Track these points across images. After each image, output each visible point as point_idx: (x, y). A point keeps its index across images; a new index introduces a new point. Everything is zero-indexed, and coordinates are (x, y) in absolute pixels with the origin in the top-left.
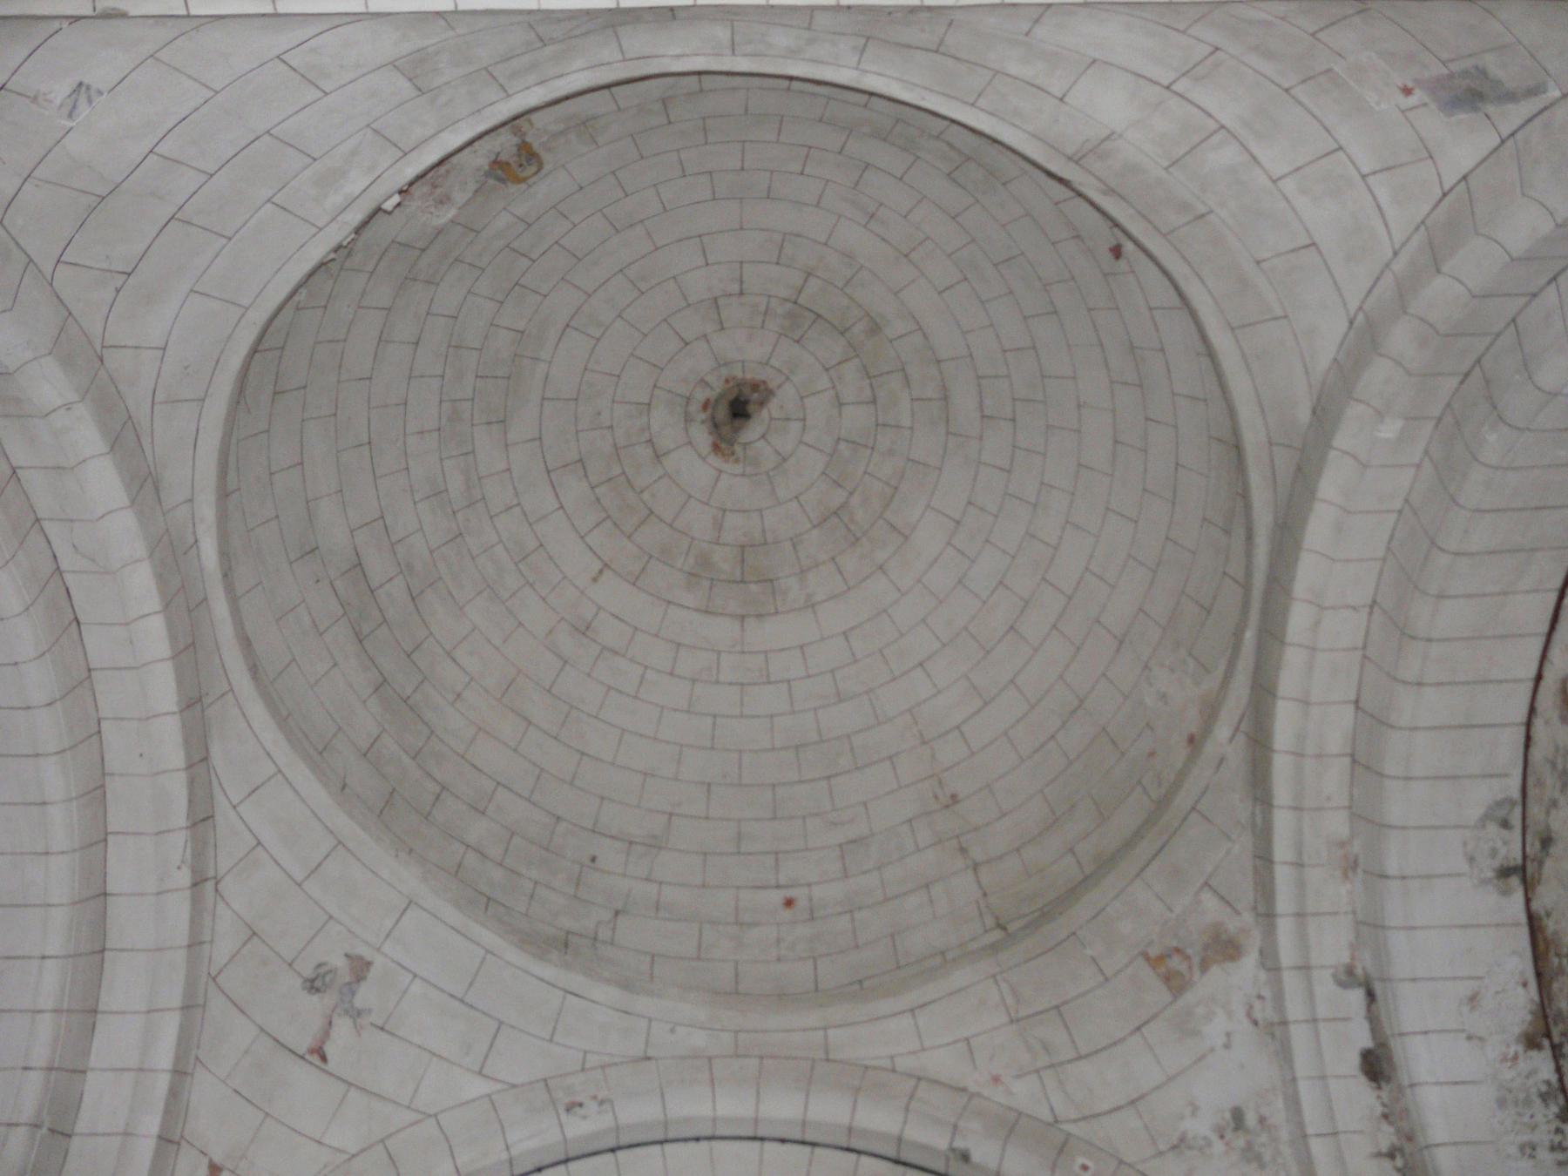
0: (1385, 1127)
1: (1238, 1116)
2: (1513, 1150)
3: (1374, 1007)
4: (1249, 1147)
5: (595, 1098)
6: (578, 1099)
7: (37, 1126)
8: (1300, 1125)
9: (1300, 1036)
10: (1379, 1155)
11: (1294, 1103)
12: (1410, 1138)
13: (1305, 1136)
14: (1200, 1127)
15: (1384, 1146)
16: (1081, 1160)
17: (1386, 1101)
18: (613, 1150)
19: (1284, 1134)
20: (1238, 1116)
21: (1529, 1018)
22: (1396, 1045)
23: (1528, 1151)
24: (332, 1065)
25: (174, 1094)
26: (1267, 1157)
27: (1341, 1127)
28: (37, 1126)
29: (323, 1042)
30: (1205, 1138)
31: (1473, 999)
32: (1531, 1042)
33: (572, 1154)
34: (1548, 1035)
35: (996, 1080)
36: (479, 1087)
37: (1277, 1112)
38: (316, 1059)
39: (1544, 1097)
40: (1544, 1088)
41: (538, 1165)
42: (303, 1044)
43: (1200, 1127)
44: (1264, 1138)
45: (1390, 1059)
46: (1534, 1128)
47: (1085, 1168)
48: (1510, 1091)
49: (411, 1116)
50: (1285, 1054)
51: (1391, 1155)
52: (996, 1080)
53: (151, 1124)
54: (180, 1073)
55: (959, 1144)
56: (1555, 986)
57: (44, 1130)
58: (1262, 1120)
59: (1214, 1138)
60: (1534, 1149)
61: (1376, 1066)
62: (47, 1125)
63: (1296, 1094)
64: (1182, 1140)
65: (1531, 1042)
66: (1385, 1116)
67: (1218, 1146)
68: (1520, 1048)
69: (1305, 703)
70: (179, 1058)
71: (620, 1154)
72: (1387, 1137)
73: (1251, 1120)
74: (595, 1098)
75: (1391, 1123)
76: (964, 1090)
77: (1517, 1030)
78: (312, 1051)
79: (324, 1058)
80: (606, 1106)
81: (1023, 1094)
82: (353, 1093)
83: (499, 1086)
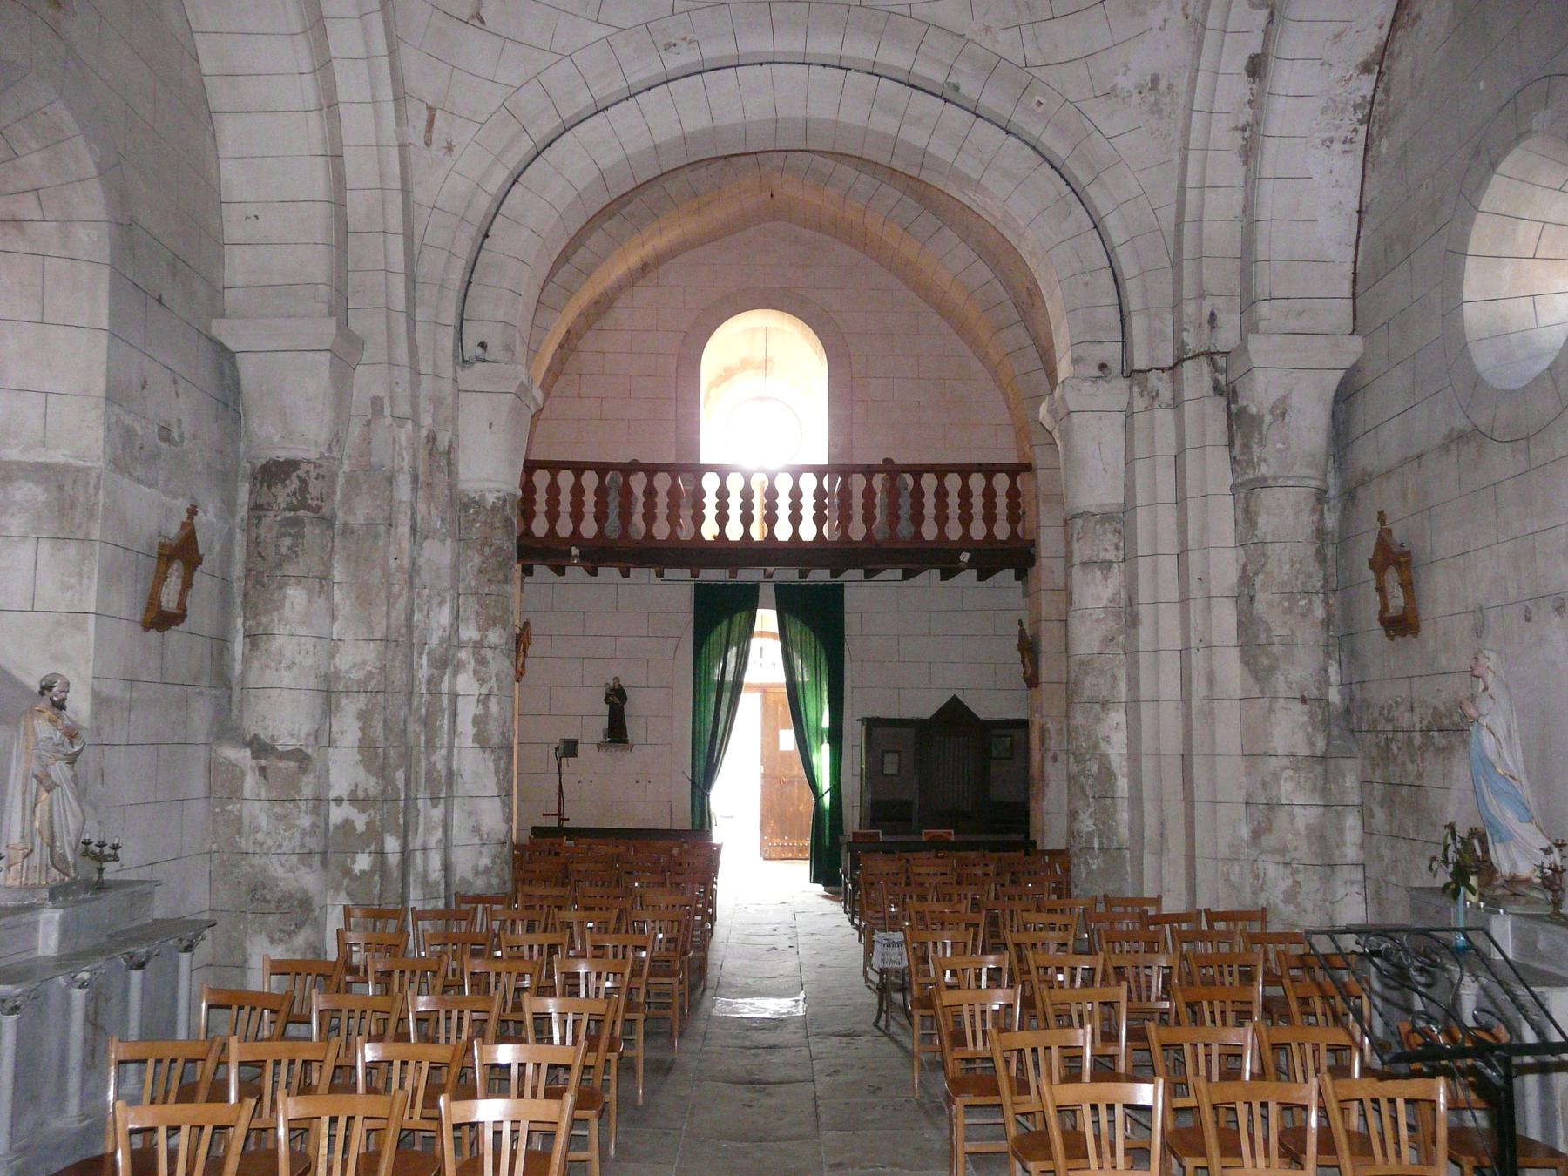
0: (1248, 110)
1: (1155, 80)
2: (1318, 142)
3: (1270, 26)
4: (1157, 103)
5: (685, 39)
6: (674, 41)
7: (321, 109)
8: (1192, 102)
9: (1210, 38)
10: (1236, 129)
11: (1193, 81)
12: (1258, 123)
13: (1192, 110)
14: (1126, 83)
15: (1242, 122)
16: (1037, 98)
17: (1254, 91)
18: (700, 73)
19: (1182, 100)
20: (1155, 80)
21: (1373, 50)
22: (1272, 62)
23: (1328, 143)
24: (489, 25)
25: (393, 68)
26: (1165, 113)
27: (1162, 647)
28: (321, 109)
29: (479, 9)
30: (1129, 91)
31: (1338, 37)
32: (1366, 68)
33: (670, 77)
34: (1380, 65)
35: (987, 29)
36: (597, 32)
37: (1181, 87)
38: (476, 22)
39: (1356, 107)
40: (1359, 100)
41: (647, 86)
42: (466, 13)
43: (1126, 83)
44: (1168, 100)
45: (1266, 66)
46: (1339, 128)
47: (1040, 103)
48: (1335, 102)
49: (552, 58)
50: (1199, 44)
51: (1244, 129)
52: (987, 29)
53: (387, 93)
54: (392, 52)
55: (953, 79)
56: (1399, 34)
57: (325, 109)
58: (1170, 87)
59: (1135, 92)
60: (1332, 142)
61: (1256, 68)
62: (325, 105)
63: (1196, 76)
64: (1113, 89)
65: (1366, 68)
66: (1250, 102)
67: (1136, 99)
68: (1355, 73)
69: (1157, 754)
70: (389, 45)
71: (704, 75)
72: (1246, 116)
73: (1163, 86)
74: (685, 39)
75: (1251, 107)
76: (962, 36)
77: (1360, 59)
78: (473, 17)
79: (482, 21)
80: (694, 45)
81: (1005, 42)
82: (509, 44)
83: (613, 30)
